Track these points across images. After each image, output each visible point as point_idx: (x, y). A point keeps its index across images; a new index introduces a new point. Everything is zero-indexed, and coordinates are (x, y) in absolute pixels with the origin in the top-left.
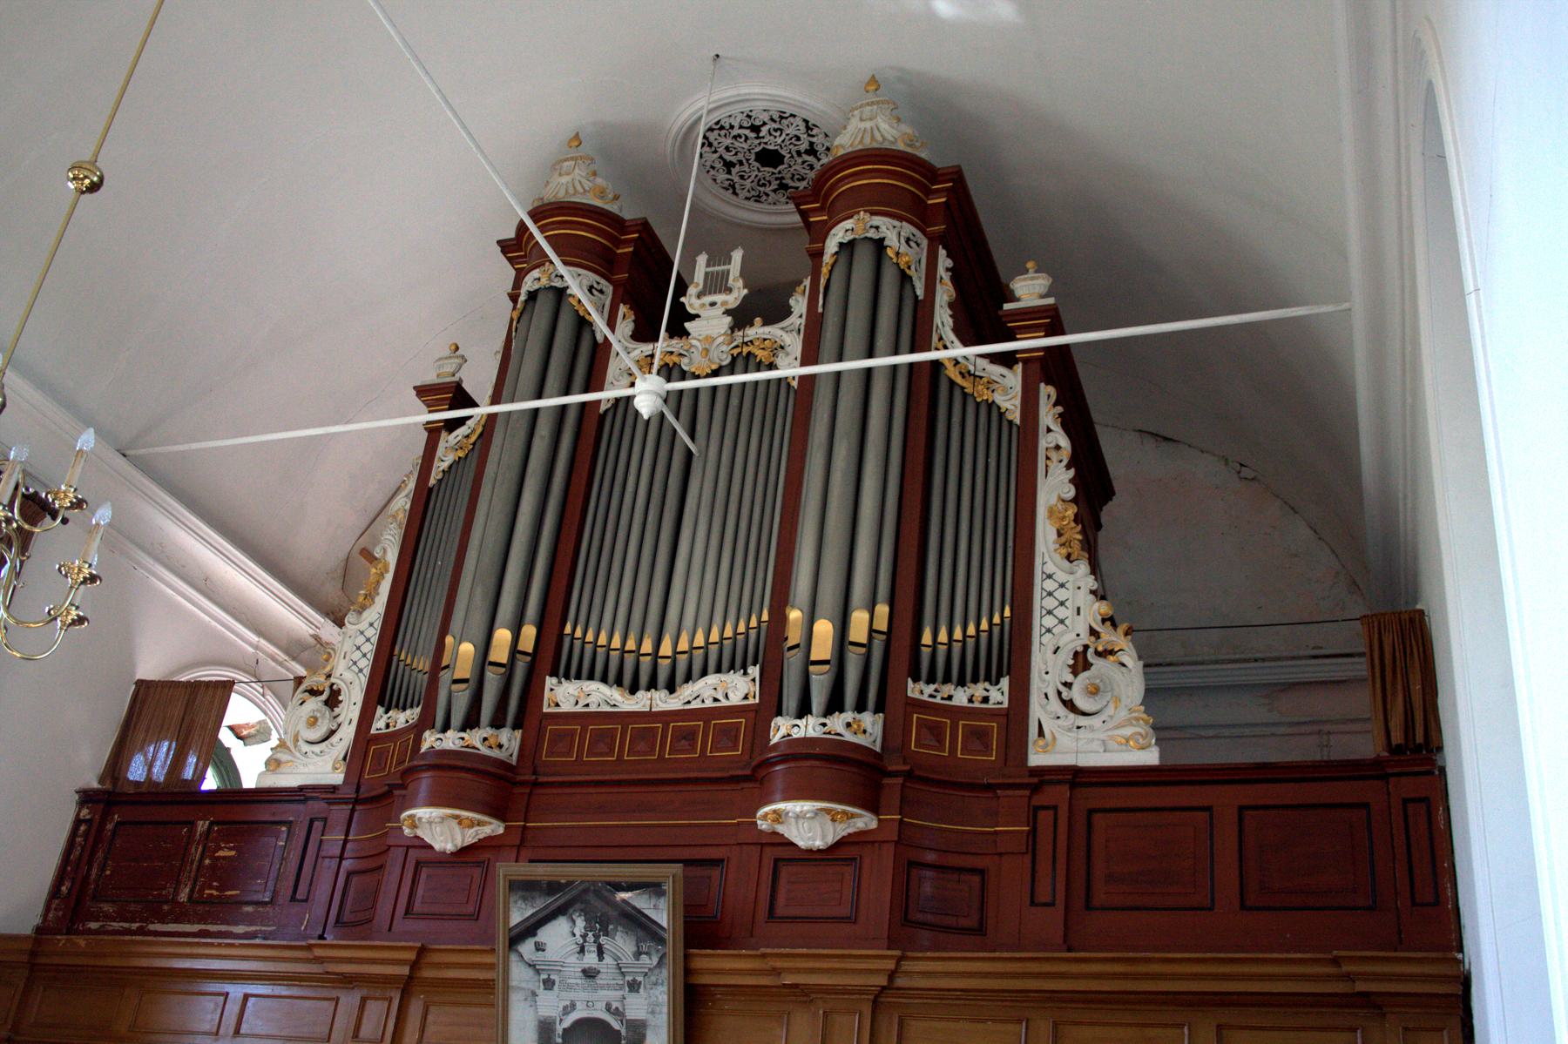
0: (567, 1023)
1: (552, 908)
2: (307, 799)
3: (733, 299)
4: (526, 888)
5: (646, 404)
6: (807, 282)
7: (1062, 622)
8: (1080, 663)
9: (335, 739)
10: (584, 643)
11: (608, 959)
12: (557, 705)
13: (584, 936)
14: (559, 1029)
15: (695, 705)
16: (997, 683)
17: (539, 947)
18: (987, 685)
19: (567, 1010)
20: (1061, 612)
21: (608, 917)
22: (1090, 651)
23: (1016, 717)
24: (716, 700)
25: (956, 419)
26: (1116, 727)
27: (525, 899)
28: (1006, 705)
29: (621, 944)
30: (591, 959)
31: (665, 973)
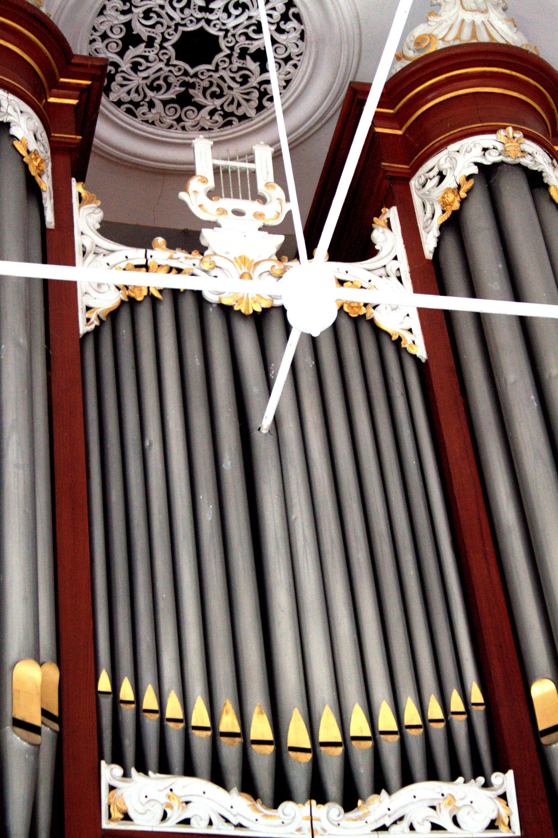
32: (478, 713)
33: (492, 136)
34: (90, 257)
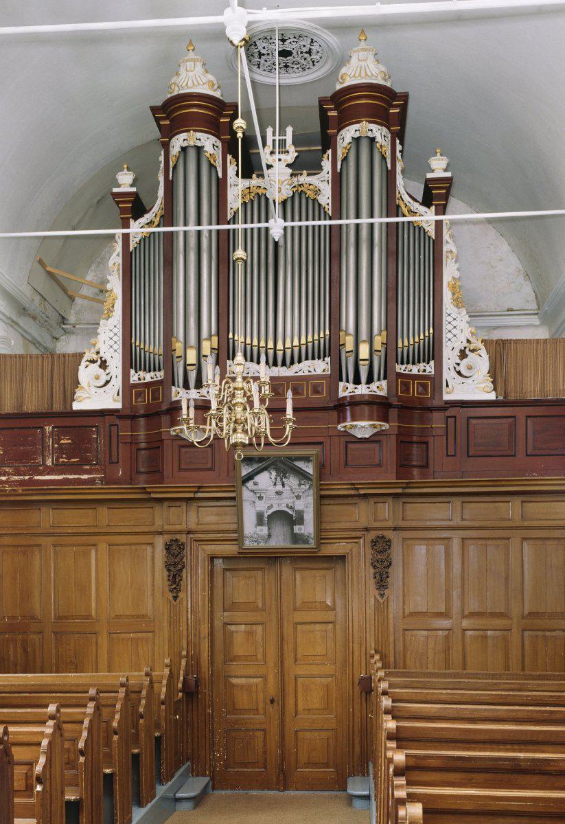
0: (270, 512)
1: (261, 468)
2: (104, 415)
3: (290, 158)
7: (455, 336)
8: (463, 355)
9: (110, 385)
11: (286, 487)
12: (234, 373)
13: (276, 479)
14: (266, 515)
15: (300, 374)
16: (428, 363)
17: (255, 484)
18: (425, 364)
19: (269, 508)
20: (454, 331)
22: (467, 350)
23: (436, 381)
24: (309, 371)
25: (406, 236)
26: (479, 384)
27: (248, 465)
28: (433, 373)
29: (292, 481)
30: (279, 487)
31: (312, 491)
32: (327, 337)
33: (358, 125)
34: (233, 187)
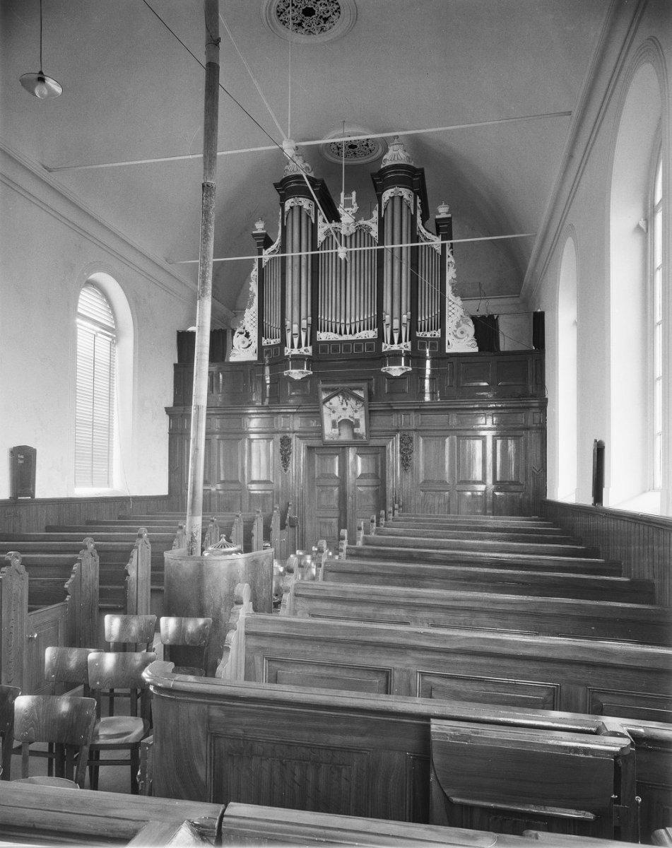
4: (326, 390)
5: (342, 255)
6: (377, 206)
8: (458, 325)
9: (251, 347)
10: (332, 322)
14: (337, 422)
17: (331, 404)
20: (453, 311)
21: (347, 394)
29: (352, 402)
30: (345, 406)
